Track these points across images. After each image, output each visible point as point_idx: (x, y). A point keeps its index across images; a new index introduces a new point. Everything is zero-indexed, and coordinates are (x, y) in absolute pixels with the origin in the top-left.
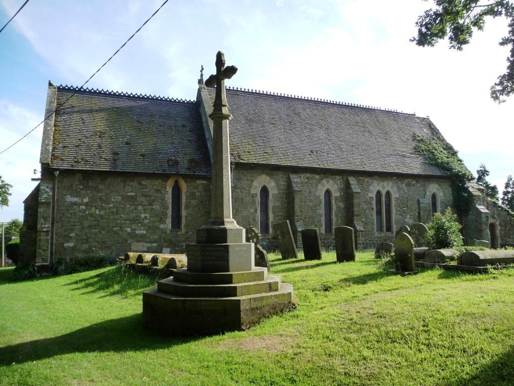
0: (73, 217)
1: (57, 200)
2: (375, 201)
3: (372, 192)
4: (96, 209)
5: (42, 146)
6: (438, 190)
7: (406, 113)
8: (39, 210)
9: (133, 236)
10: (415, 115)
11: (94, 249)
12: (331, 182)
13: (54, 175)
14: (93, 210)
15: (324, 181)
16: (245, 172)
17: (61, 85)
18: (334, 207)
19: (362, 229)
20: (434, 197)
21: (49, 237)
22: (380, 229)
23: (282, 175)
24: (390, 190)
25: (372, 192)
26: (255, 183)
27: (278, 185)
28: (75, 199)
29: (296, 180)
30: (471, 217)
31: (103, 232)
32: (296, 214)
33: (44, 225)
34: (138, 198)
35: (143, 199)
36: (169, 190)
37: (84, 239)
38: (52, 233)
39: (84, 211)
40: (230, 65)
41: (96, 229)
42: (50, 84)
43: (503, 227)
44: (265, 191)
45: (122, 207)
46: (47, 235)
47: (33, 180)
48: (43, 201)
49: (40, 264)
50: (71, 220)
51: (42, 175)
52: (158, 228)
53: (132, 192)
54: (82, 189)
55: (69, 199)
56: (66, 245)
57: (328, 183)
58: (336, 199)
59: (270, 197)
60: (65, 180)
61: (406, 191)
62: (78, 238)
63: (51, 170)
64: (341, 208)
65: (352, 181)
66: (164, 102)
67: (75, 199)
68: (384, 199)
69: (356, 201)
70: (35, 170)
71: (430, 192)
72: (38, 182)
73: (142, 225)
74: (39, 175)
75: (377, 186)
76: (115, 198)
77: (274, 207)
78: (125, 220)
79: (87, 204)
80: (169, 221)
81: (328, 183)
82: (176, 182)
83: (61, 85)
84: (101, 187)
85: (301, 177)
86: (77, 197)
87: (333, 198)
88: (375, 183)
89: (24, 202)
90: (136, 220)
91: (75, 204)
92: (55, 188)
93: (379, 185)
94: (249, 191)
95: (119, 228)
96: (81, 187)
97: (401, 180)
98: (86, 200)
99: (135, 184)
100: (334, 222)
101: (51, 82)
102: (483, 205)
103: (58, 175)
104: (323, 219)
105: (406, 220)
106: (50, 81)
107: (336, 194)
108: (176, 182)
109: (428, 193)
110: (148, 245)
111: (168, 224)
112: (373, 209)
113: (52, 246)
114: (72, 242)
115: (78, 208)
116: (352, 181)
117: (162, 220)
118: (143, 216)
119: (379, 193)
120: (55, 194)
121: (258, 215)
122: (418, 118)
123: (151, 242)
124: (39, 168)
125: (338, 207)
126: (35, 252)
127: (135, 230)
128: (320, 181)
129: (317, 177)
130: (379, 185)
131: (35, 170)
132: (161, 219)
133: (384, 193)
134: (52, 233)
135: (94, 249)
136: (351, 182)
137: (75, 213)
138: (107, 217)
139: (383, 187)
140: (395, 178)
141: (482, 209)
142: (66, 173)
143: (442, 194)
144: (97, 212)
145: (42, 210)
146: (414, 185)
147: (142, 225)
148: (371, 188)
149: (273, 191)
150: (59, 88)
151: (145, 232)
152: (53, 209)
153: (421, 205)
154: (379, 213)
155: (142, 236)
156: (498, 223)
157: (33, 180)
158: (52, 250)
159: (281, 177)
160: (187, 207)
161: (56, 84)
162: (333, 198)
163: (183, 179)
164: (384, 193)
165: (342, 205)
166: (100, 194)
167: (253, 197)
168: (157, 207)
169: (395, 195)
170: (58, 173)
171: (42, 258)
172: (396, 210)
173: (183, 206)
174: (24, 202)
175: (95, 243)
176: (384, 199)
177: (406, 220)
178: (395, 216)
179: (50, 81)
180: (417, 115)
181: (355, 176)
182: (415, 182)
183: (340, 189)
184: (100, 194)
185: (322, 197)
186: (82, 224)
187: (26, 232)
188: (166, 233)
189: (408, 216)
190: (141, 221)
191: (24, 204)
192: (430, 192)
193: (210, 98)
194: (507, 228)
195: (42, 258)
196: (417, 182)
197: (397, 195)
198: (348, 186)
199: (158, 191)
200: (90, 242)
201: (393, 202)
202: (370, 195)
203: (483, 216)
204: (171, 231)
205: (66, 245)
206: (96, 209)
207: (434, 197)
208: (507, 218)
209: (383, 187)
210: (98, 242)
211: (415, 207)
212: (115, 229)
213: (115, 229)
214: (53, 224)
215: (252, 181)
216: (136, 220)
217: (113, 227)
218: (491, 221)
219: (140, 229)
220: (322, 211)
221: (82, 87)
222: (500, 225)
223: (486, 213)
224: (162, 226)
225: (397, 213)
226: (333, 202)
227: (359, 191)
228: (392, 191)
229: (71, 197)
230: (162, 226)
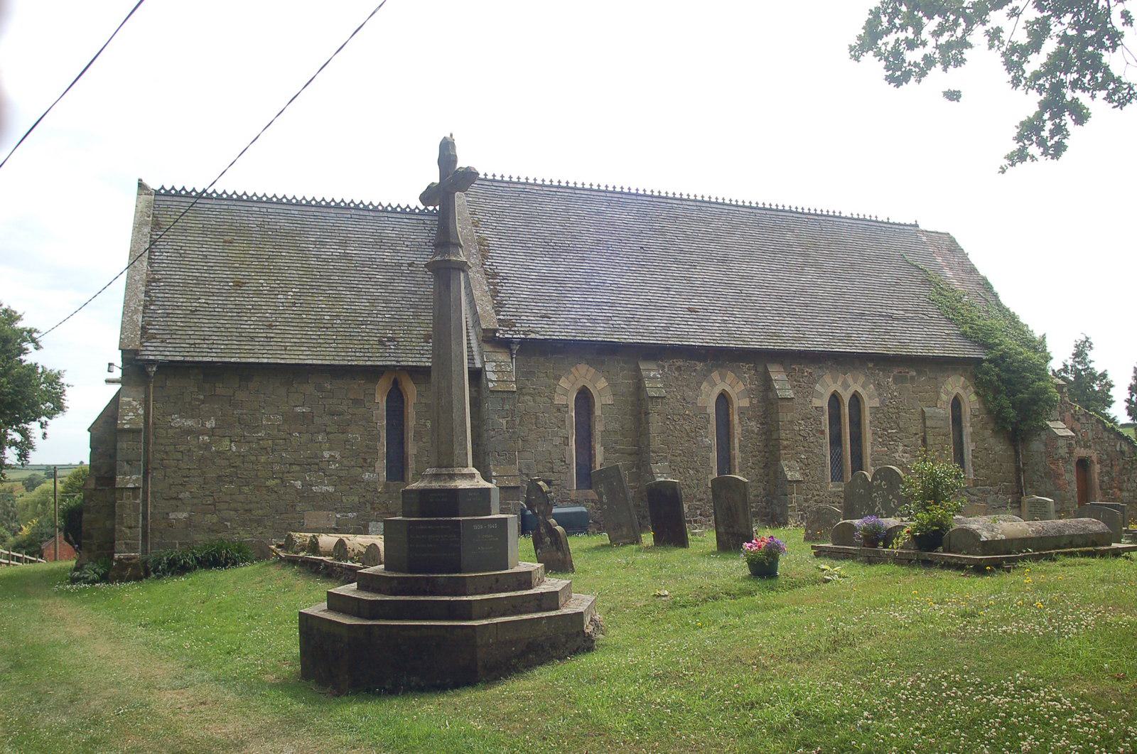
0: (186, 458)
1: (154, 424)
2: (827, 416)
3: (820, 396)
4: (231, 442)
5: (123, 313)
6: (965, 388)
7: (897, 222)
8: (119, 445)
9: (306, 495)
10: (917, 226)
11: (229, 524)
12: (730, 376)
13: (147, 375)
14: (226, 442)
15: (715, 375)
16: (542, 359)
17: (163, 188)
18: (737, 430)
19: (798, 476)
20: (956, 403)
21: (138, 501)
22: (838, 475)
23: (622, 364)
24: (860, 390)
25: (820, 396)
26: (563, 383)
27: (613, 385)
28: (189, 423)
29: (652, 374)
30: (1036, 446)
31: (246, 489)
32: (652, 447)
33: (129, 480)
34: (316, 419)
35: (326, 419)
36: (381, 400)
37: (210, 505)
38: (145, 493)
39: (207, 447)
40: (465, 166)
41: (231, 483)
42: (141, 185)
43: (1106, 466)
44: (585, 398)
45: (283, 437)
46: (136, 497)
47: (108, 381)
48: (126, 426)
49: (122, 556)
50: (182, 465)
51: (123, 375)
52: (357, 481)
53: (303, 406)
54: (203, 402)
55: (178, 421)
56: (172, 516)
57: (723, 378)
58: (742, 411)
59: (598, 412)
60: (168, 383)
61: (895, 394)
62: (196, 501)
63: (141, 363)
64: (753, 432)
65: (778, 376)
66: (371, 213)
67: (189, 423)
68: (846, 410)
69: (785, 417)
70: (110, 364)
71: (947, 393)
72: (118, 386)
73: (326, 475)
74: (117, 374)
75: (828, 385)
76: (269, 419)
77: (606, 432)
78: (290, 464)
79: (211, 433)
80: (381, 465)
81: (723, 378)
82: (396, 383)
83: (163, 188)
84: (241, 396)
85: (664, 367)
86: (192, 417)
87: (736, 413)
88: (828, 378)
89: (89, 430)
90: (313, 464)
91: (189, 431)
92: (149, 401)
93: (835, 382)
94: (552, 399)
95: (278, 481)
96: (202, 397)
97: (883, 371)
98: (210, 424)
99: (309, 388)
100: (737, 463)
101: (145, 181)
102: (1063, 420)
103: (156, 372)
104: (714, 455)
105: (896, 455)
106: (140, 180)
107: (740, 402)
108: (396, 383)
109: (944, 397)
110: (338, 516)
111: (379, 472)
112: (822, 432)
113: (145, 518)
114: (184, 511)
115: (196, 439)
116: (778, 376)
117: (368, 465)
118: (326, 454)
119: (835, 399)
120: (149, 413)
121: (571, 450)
122: (925, 232)
123: (345, 510)
124: (118, 360)
125: (747, 433)
126: (113, 530)
127: (311, 485)
128: (706, 375)
129: (700, 366)
130: (835, 382)
131: (110, 364)
132: (365, 460)
133: (846, 397)
134: (145, 493)
135: (229, 524)
136: (774, 376)
137: (189, 451)
138: (253, 458)
139: (846, 386)
140: (870, 365)
141: (1060, 429)
142: (172, 369)
143: (602, 383)
144: (234, 449)
145: (125, 446)
146: (912, 378)
147: (326, 475)
148: (818, 387)
149: (603, 397)
150: (157, 193)
151: (331, 489)
152: (147, 443)
153: (928, 423)
154: (836, 441)
155: (325, 495)
156: (1095, 458)
157: (108, 381)
158: (145, 527)
159: (746, 369)
160: (418, 436)
161: (154, 185)
162: (736, 413)
163: (412, 379)
164: (846, 397)
165: (754, 426)
166: (239, 411)
167: (559, 410)
168: (355, 435)
169: (870, 402)
170: (154, 369)
171: (126, 544)
172: (874, 433)
173: (411, 434)
174: (89, 430)
175: (232, 513)
176: (846, 410)
177: (896, 455)
178: (872, 448)
179: (140, 180)
180: (922, 227)
181: (782, 363)
182: (915, 374)
183: (749, 393)
184: (239, 411)
185: (712, 410)
186: (204, 473)
187: (95, 490)
188: (376, 490)
189: (901, 448)
190: (323, 465)
191: (89, 434)
192: (947, 393)
193: (468, 201)
194: (1116, 469)
195: (126, 544)
196: (919, 373)
197: (876, 403)
198: (767, 383)
199: (356, 402)
200: (219, 511)
201: (867, 417)
202: (817, 402)
203: (1061, 443)
204: (386, 486)
205: (172, 516)
206: (231, 442)
207: (956, 403)
208: (1115, 446)
209: (846, 386)
210: (236, 510)
211: (915, 427)
212: (271, 483)
213: (271, 483)
214: (146, 474)
215: (558, 378)
216: (313, 464)
217: (267, 479)
218: (1081, 452)
219: (322, 483)
220: (711, 440)
221: (205, 191)
222: (1100, 461)
223: (1068, 436)
224: (367, 476)
225: (875, 440)
226: (735, 419)
227: (790, 394)
228: (733, 393)
229: (181, 417)
230: (367, 476)
